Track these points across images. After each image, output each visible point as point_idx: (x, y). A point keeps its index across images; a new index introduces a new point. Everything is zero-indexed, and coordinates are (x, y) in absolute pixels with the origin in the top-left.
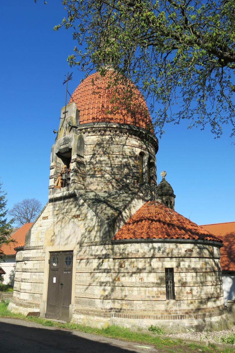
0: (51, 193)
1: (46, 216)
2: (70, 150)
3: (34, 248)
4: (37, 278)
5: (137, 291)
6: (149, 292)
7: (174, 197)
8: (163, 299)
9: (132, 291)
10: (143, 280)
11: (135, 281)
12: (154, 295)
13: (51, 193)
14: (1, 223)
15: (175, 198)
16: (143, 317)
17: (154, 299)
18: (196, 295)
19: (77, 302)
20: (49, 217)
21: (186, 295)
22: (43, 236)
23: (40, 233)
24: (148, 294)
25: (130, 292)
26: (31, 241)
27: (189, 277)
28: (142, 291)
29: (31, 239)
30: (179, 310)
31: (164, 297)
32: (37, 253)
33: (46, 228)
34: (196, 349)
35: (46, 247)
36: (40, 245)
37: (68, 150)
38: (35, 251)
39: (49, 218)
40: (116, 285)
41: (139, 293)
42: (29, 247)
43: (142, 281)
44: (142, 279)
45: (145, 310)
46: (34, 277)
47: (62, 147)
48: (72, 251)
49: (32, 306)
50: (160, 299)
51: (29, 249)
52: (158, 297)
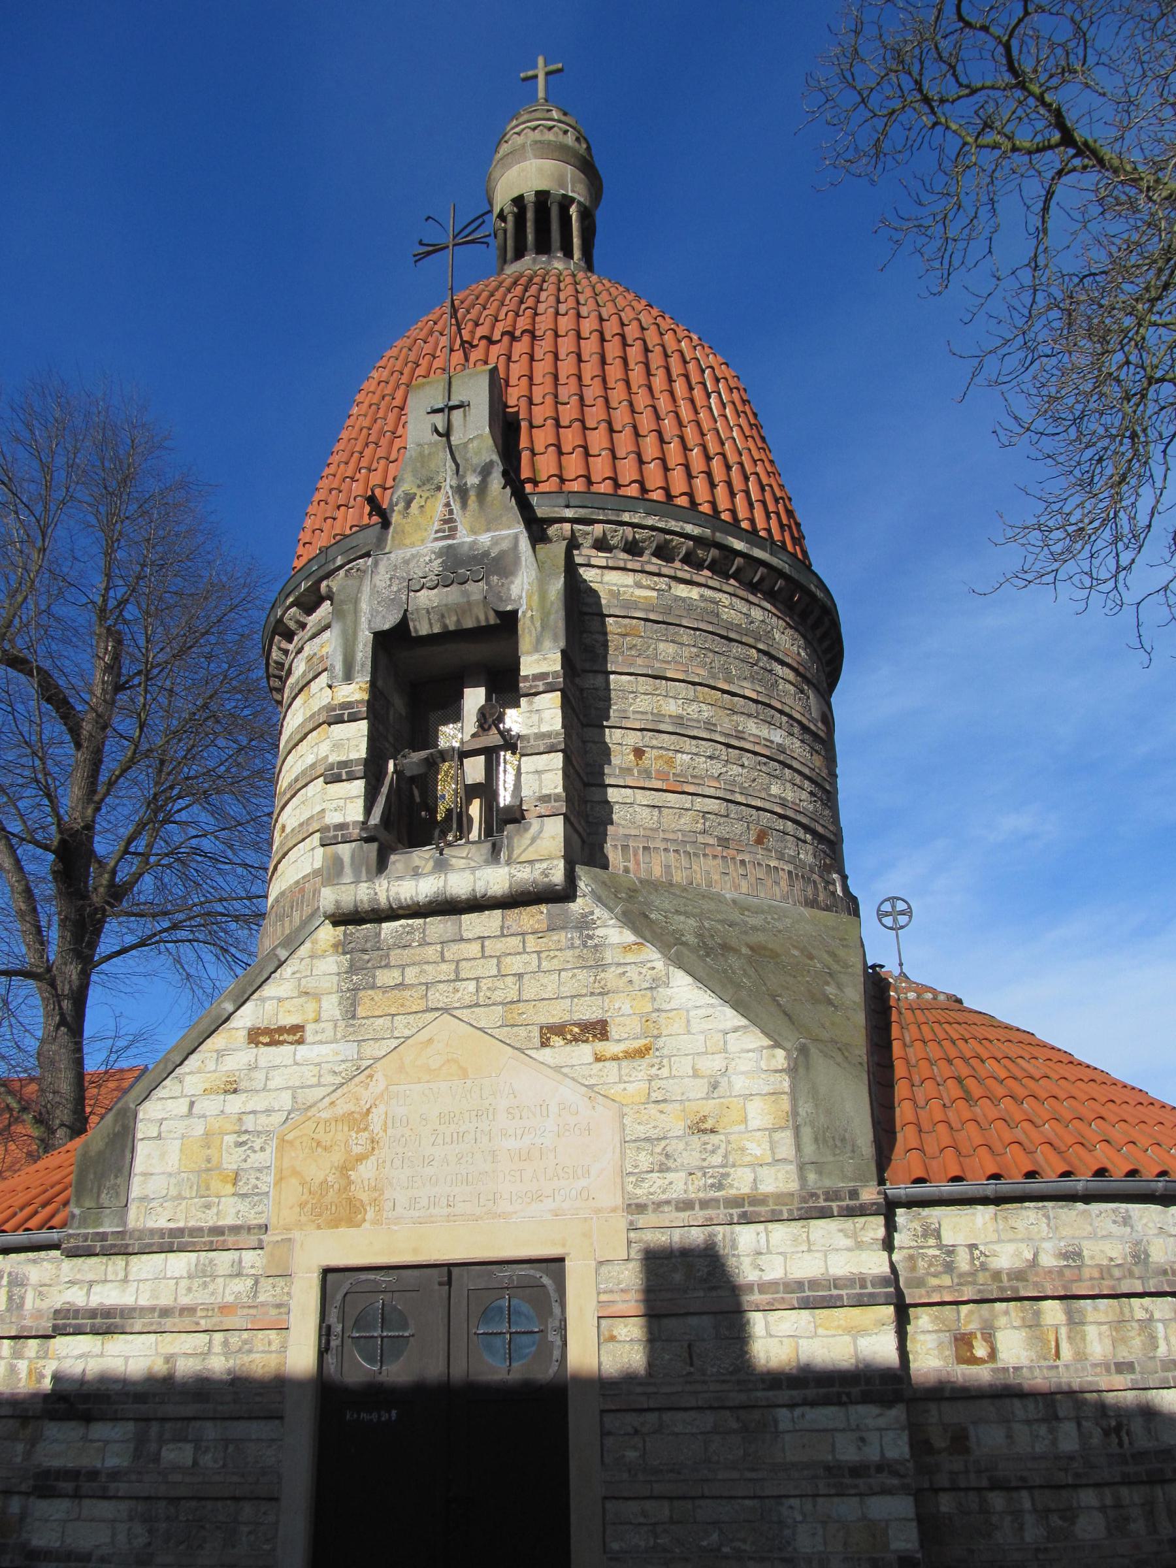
0: (348, 870)
1: (288, 1020)
2: (509, 621)
3: (170, 1242)
4: (207, 1460)
5: (1103, 1509)
9: (1070, 1514)
10: (1126, 1439)
11: (1077, 1447)
13: (348, 870)
14: (942, 2)
20: (309, 1028)
22: (257, 1159)
23: (230, 1139)
25: (1055, 1521)
26: (137, 1189)
27: (928, 1337)
29: (136, 1181)
32: (204, 1274)
33: (285, 1100)
35: (296, 1235)
36: (229, 1221)
37: (493, 620)
38: (179, 1263)
39: (309, 1035)
40: (943, 1480)
42: (121, 1234)
43: (1121, 1444)
44: (1118, 1429)
46: (177, 1455)
47: (425, 598)
51: (120, 1247)
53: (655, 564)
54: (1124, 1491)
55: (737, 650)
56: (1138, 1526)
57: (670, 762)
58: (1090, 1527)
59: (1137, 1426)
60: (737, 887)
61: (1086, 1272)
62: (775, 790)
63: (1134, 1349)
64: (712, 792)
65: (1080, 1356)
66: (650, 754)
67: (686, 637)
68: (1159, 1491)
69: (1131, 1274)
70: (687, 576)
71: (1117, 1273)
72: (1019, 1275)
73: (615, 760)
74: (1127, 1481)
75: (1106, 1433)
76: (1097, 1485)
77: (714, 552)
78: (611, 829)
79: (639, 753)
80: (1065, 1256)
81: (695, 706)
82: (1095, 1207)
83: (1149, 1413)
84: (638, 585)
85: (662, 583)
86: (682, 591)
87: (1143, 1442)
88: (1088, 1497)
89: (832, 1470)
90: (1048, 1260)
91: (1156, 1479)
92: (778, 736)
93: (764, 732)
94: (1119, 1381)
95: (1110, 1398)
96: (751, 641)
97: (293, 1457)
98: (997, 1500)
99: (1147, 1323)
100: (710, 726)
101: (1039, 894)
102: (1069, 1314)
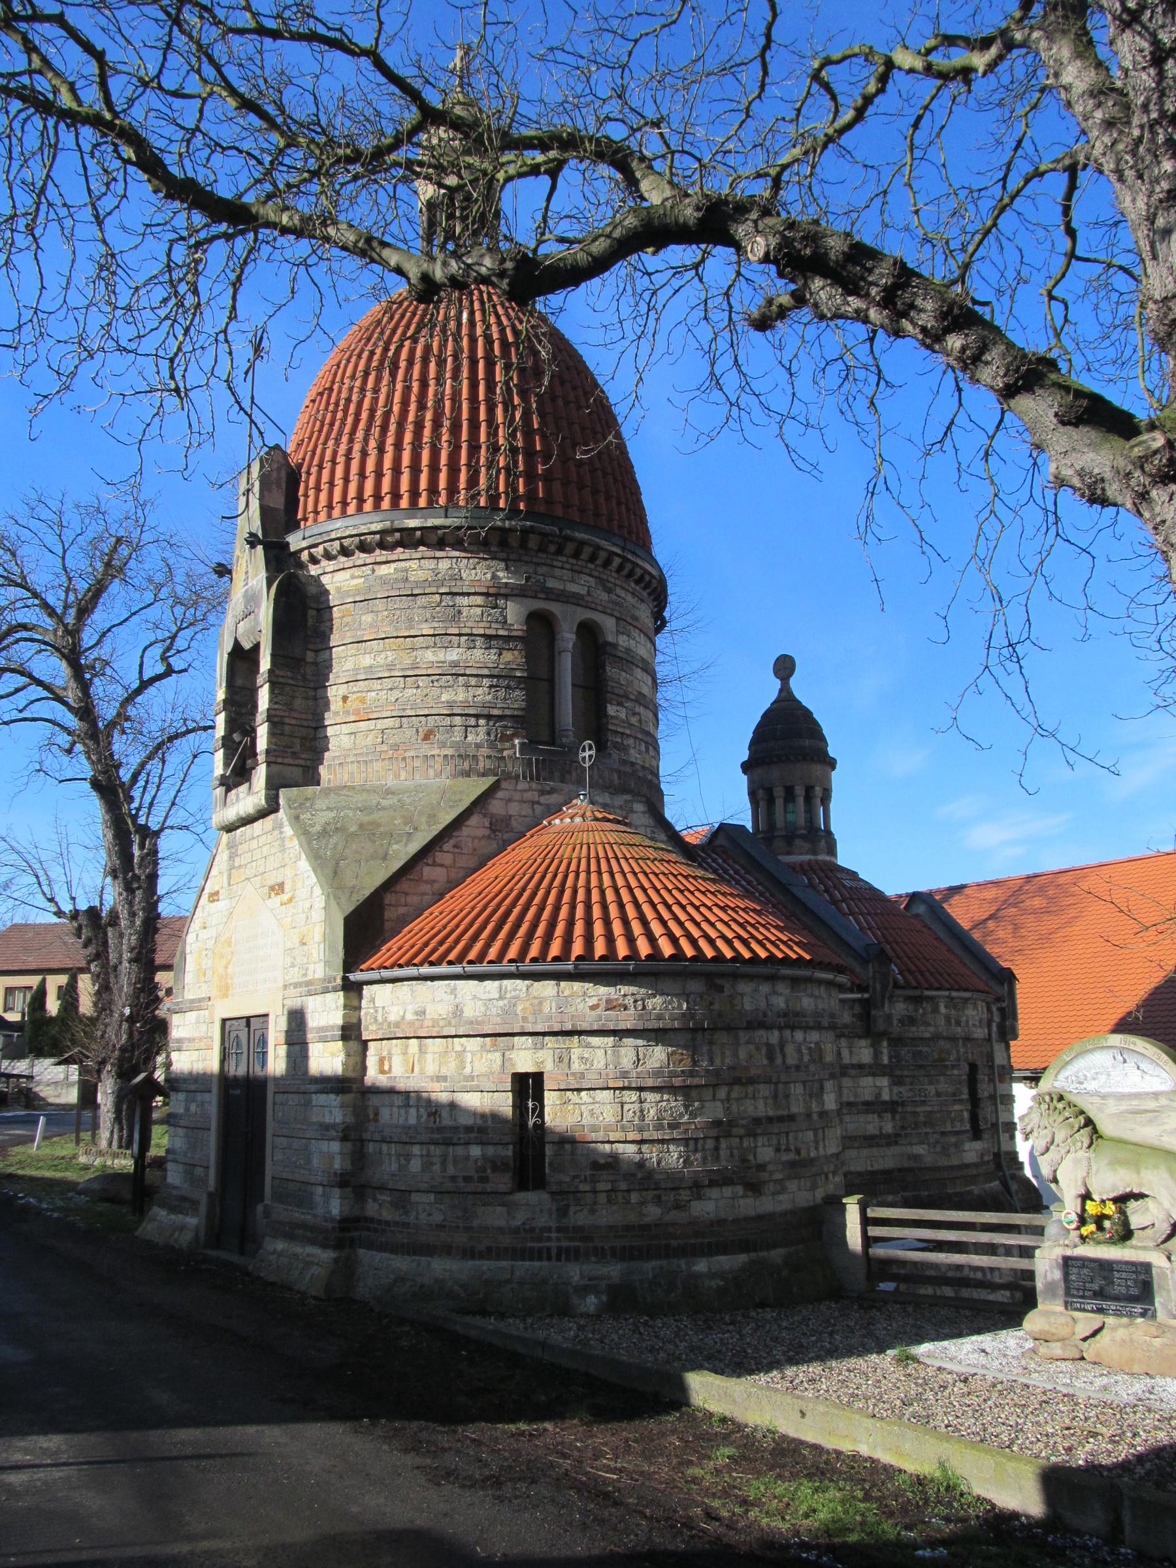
6: (455, 1162)
7: (832, 764)
8: (502, 1188)
9: (408, 1157)
12: (473, 1173)
15: (833, 767)
16: (428, 1250)
17: (470, 1187)
18: (634, 1175)
19: (279, 1197)
21: (588, 1173)
24: (451, 1170)
25: (403, 1161)
28: (435, 1160)
30: (559, 1230)
31: (502, 1182)
34: (668, 1362)
41: (427, 1166)
45: (440, 1227)
48: (267, 1015)
49: (974, 1177)
50: (489, 1187)
52: (484, 1180)
53: (360, 557)
54: (432, 1148)
55: (422, 601)
56: (437, 1168)
57: (363, 701)
58: (415, 1165)
59: (445, 1114)
60: (397, 776)
61: (426, 1023)
62: (444, 698)
63: (450, 1069)
64: (388, 714)
65: (422, 1072)
66: (352, 697)
67: (380, 605)
68: (451, 1149)
69: (450, 1024)
70: (383, 559)
71: (442, 1023)
72: (397, 1025)
73: (332, 707)
74: (436, 1144)
75: (429, 1115)
76: (421, 1143)
77: (397, 535)
78: (326, 754)
79: (345, 699)
80: (416, 1013)
81: (383, 656)
82: (436, 983)
83: (453, 1106)
84: (353, 577)
85: (367, 570)
86: (384, 570)
87: (447, 1121)
88: (416, 1150)
89: (866, 1138)
90: (410, 1017)
91: (448, 1143)
92: (453, 655)
93: (441, 655)
94: (437, 1086)
95: (433, 1096)
96: (434, 590)
97: (212, 1102)
98: (385, 1147)
99: (461, 1055)
100: (391, 667)
101: (289, 800)
102: (420, 1047)
